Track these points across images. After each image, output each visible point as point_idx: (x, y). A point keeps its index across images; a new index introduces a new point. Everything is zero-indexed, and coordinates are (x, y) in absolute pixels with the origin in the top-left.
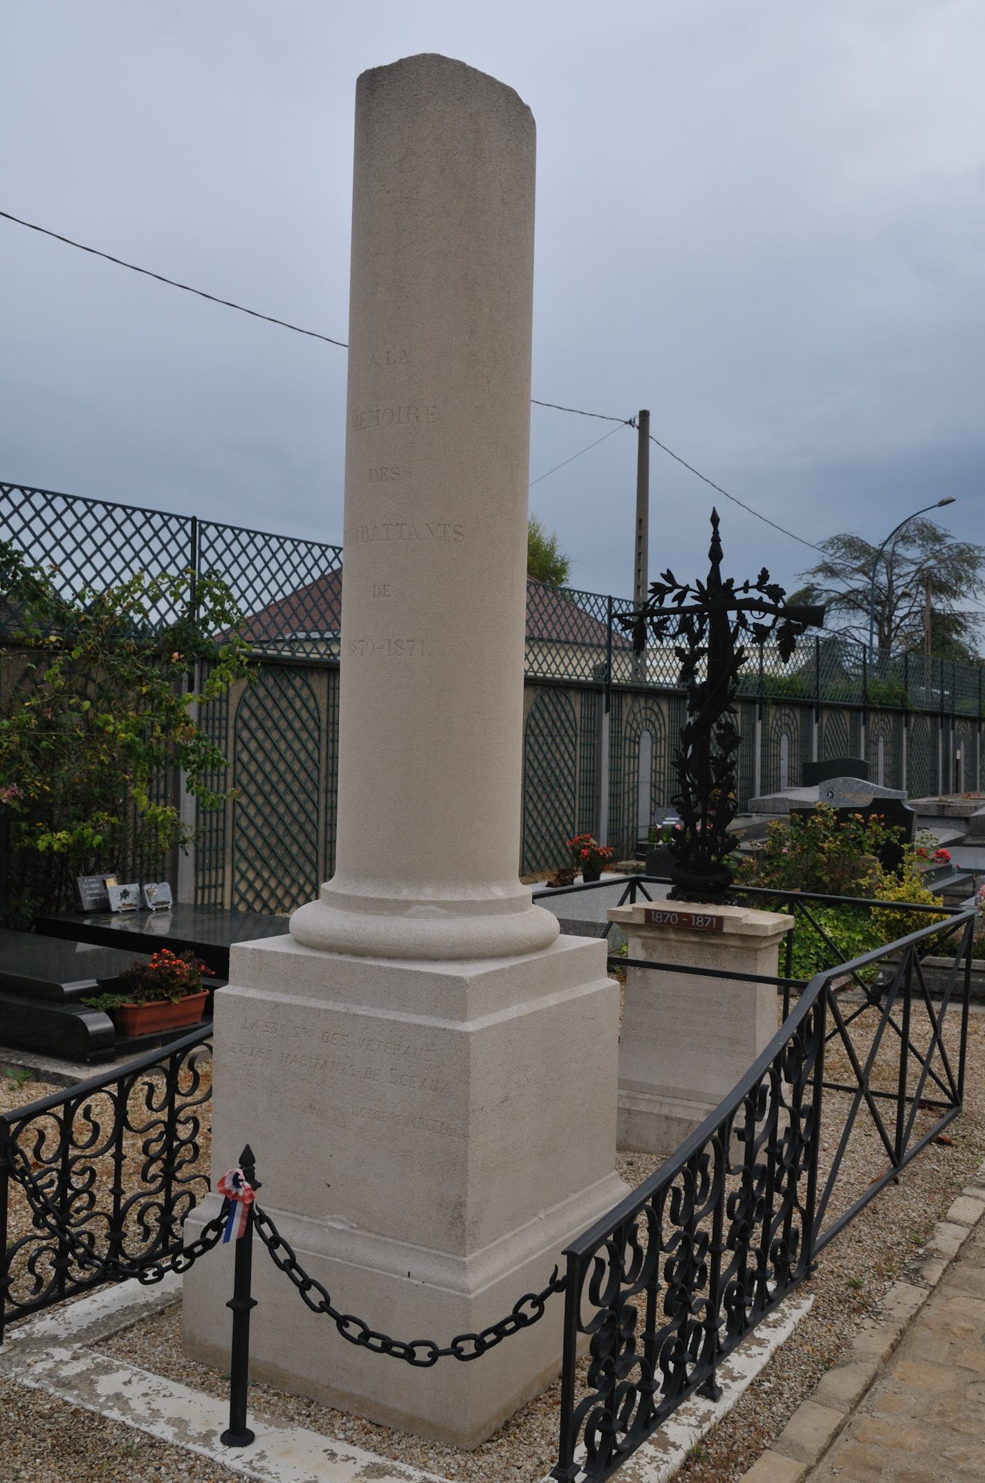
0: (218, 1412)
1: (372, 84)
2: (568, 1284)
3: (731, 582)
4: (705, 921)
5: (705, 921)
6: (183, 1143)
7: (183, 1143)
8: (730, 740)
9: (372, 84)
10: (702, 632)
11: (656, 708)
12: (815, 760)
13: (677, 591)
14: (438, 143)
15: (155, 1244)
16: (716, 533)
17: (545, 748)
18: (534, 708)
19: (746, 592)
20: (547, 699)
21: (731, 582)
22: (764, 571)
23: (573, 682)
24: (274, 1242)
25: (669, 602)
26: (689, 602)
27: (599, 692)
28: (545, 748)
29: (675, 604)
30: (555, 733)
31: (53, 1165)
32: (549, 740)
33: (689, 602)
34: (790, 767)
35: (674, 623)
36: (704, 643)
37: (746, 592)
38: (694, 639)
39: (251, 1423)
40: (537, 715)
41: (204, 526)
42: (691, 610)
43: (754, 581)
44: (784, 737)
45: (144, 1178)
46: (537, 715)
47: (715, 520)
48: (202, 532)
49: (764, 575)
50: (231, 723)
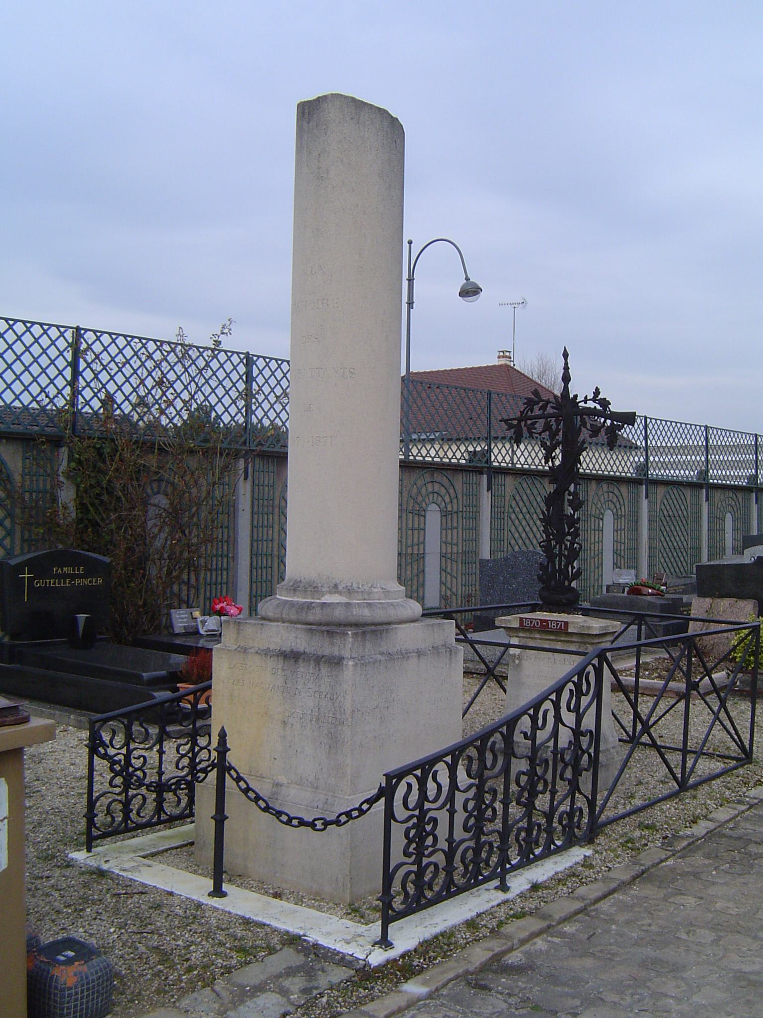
0: (209, 884)
1: (309, 112)
2: (387, 792)
3: (576, 396)
4: (557, 625)
5: (557, 625)
6: (202, 749)
7: (202, 749)
8: (577, 504)
9: (309, 112)
10: (558, 430)
11: (616, 491)
12: (755, 533)
13: (541, 404)
14: (349, 145)
15: (185, 809)
16: (566, 363)
17: (524, 523)
18: (515, 492)
19: (586, 403)
20: (525, 485)
21: (576, 396)
22: (597, 389)
23: (594, 475)
24: (239, 779)
25: (537, 412)
26: (549, 410)
27: (702, 488)
28: (524, 523)
29: (540, 412)
30: (532, 510)
31: (135, 792)
32: (528, 516)
33: (549, 410)
34: (734, 539)
35: (540, 425)
36: (560, 437)
37: (586, 403)
38: (553, 436)
39: (225, 887)
40: (518, 498)
41: (255, 358)
42: (551, 416)
43: (591, 396)
44: (729, 516)
45: (177, 767)
46: (518, 498)
47: (566, 355)
48: (254, 363)
49: (597, 392)
50: (277, 502)
